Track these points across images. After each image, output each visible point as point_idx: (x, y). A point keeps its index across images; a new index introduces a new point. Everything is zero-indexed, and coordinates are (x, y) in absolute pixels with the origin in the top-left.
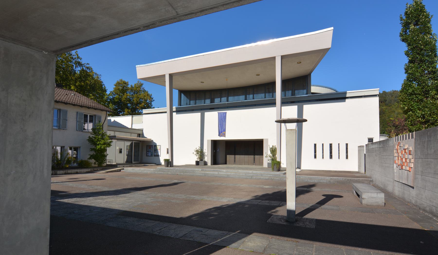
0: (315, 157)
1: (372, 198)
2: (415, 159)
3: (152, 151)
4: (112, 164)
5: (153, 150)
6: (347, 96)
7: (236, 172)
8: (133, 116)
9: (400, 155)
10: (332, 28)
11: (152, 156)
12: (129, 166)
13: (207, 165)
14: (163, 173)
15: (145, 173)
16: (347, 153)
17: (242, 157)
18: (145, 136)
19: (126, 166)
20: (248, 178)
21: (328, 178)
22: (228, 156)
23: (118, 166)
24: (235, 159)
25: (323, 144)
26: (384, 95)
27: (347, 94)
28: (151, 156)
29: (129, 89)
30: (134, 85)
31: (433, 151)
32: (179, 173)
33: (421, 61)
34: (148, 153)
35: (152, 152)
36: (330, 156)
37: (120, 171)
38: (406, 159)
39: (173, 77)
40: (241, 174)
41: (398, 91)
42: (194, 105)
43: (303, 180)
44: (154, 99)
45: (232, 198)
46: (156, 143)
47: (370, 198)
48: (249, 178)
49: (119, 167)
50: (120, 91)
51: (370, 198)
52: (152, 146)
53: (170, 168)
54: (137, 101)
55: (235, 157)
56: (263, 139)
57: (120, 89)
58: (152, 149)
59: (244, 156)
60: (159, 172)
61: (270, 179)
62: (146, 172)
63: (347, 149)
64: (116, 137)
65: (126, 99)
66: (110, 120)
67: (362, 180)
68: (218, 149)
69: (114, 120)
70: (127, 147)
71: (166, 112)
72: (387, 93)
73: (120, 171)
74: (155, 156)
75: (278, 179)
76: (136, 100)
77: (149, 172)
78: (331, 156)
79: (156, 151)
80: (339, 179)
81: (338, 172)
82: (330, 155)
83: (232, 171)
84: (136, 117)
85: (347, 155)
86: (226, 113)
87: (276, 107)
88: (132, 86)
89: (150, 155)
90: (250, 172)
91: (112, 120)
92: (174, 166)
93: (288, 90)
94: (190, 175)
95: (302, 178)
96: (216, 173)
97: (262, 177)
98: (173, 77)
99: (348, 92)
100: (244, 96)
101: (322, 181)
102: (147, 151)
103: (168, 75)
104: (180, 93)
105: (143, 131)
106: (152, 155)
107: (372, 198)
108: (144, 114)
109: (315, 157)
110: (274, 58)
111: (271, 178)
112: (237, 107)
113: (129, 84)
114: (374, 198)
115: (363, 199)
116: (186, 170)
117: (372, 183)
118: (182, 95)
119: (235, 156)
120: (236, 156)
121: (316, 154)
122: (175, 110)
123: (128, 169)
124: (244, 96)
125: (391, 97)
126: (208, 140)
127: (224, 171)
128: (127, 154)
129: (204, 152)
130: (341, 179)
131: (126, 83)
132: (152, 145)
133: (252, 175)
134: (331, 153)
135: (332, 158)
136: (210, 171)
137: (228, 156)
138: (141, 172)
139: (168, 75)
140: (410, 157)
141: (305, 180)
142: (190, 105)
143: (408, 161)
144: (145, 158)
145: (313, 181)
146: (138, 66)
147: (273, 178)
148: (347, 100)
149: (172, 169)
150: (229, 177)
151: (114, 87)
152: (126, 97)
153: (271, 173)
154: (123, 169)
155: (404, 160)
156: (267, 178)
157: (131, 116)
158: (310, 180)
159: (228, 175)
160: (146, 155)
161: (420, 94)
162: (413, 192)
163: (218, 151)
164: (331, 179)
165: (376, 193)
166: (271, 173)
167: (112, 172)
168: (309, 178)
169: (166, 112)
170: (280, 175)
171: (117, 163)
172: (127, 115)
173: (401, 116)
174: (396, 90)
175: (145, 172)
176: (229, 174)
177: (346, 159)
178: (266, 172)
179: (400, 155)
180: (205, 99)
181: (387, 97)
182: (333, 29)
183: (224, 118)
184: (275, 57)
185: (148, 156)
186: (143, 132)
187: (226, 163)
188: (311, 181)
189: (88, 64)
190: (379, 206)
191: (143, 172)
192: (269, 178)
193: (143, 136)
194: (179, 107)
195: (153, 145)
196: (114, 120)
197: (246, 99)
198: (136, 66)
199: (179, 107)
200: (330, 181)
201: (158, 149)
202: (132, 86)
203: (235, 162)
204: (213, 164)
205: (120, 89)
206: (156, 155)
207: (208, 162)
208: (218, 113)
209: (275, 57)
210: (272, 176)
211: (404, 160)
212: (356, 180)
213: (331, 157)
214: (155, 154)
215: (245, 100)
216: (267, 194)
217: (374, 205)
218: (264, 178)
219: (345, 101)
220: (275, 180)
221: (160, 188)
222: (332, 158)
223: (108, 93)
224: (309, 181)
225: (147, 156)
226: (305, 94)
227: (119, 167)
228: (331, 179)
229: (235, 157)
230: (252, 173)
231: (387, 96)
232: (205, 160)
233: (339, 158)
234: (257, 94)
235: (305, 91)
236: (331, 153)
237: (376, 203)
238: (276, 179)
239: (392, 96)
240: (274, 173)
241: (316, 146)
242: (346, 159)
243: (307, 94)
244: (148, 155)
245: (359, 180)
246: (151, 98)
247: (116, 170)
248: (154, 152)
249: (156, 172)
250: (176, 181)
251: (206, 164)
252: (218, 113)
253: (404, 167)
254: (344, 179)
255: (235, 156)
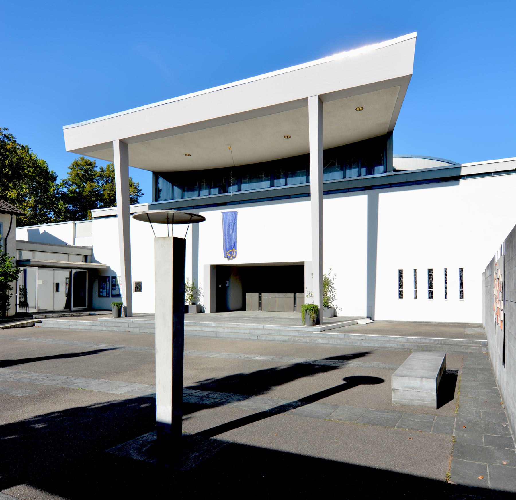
0: (401, 296)
1: (411, 388)
3: (108, 288)
4: (27, 312)
5: (109, 285)
6: (462, 174)
7: (235, 326)
8: (76, 222)
10: (414, 34)
11: (109, 297)
12: (57, 316)
13: (204, 312)
14: (104, 329)
15: (74, 329)
16: (462, 288)
17: (273, 296)
18: (97, 258)
19: (51, 316)
20: (252, 338)
21: (402, 339)
22: (248, 295)
23: (33, 315)
24: (260, 300)
25: (415, 271)
27: (463, 169)
28: (106, 297)
29: (95, 175)
30: (106, 167)
32: (131, 330)
34: (101, 290)
35: (109, 289)
36: (429, 293)
37: (34, 325)
39: (130, 146)
40: (242, 331)
42: (179, 200)
43: (352, 343)
44: (142, 192)
45: (147, 385)
46: (115, 272)
47: (406, 389)
48: (254, 338)
49: (36, 318)
50: (80, 178)
51: (406, 389)
52: (109, 277)
53: (127, 319)
54: (110, 195)
55: (260, 297)
56: (304, 262)
57: (81, 175)
58: (108, 283)
59: (276, 294)
60: (98, 328)
61: (292, 340)
62: (75, 328)
63: (461, 278)
64: (30, 261)
65: (90, 192)
66: (38, 230)
67: (468, 342)
68: (228, 282)
69: (45, 231)
70: (66, 280)
71: (115, 216)
73: (34, 325)
74: (113, 296)
75: (306, 340)
76: (109, 194)
77: (81, 327)
78: (430, 294)
79: (115, 287)
80: (423, 341)
81: (435, 325)
82: (429, 291)
83: (229, 326)
84: (81, 225)
85: (462, 291)
86: (236, 214)
87: (310, 200)
88: (102, 169)
89: (105, 294)
90: (260, 326)
91: (41, 231)
92: (133, 315)
93: (350, 168)
94: (150, 333)
95: (353, 338)
96: (198, 329)
97: (277, 338)
98: (129, 146)
99: (463, 165)
100: (269, 182)
101: (388, 345)
102: (99, 288)
103: (118, 141)
104: (155, 178)
105: (93, 250)
106: (109, 294)
107: (411, 388)
108: (95, 217)
109: (401, 296)
110: (305, 101)
111: (293, 338)
112: (240, 202)
113: (96, 165)
114: (415, 390)
115: (394, 390)
116: (146, 322)
117: (486, 349)
118: (161, 180)
119: (295, 294)
120: (263, 295)
121: (402, 291)
123: (48, 322)
124: (269, 182)
126: (205, 266)
127: (214, 324)
128: (67, 293)
129: (198, 288)
130: (428, 341)
131: (90, 164)
132: (109, 276)
133: (260, 332)
134: (431, 287)
135: (432, 298)
136: (189, 324)
137: (248, 295)
138: (68, 327)
139: (118, 142)
141: (356, 343)
142: (173, 199)
144: (97, 301)
145: (370, 345)
146: (67, 126)
147: (297, 339)
148: (462, 182)
149: (124, 321)
150: (217, 337)
151: (69, 171)
152: (90, 189)
153: (298, 328)
154: (41, 322)
156: (286, 338)
157: (72, 222)
158: (365, 343)
159: (217, 333)
160: (97, 294)
163: (227, 285)
164: (408, 340)
165: (420, 379)
166: (298, 328)
167: (16, 327)
168: (366, 339)
169: (115, 216)
170: (311, 332)
171: (39, 310)
172: (65, 220)
175: (75, 327)
176: (221, 330)
177: (460, 298)
178: (289, 327)
180: (200, 189)
182: (416, 36)
183: (232, 222)
184: (308, 98)
185: (102, 296)
186: (92, 253)
187: (243, 308)
188: (368, 345)
189: (5, 129)
190: (425, 407)
191: (71, 327)
192: (291, 339)
193: (93, 260)
194: (155, 203)
195: (111, 275)
196: (45, 231)
197: (272, 186)
198: (64, 127)
199: (155, 203)
200: (403, 345)
201: (119, 283)
202: (102, 169)
203: (260, 306)
204: (215, 311)
205: (81, 175)
206: (115, 294)
207: (205, 306)
208: (222, 213)
209: (308, 98)
210: (297, 334)
212: (455, 343)
213: (430, 295)
214: (114, 293)
215: (271, 187)
216: (241, 374)
217: (416, 404)
218: (282, 339)
219: (458, 184)
220: (300, 342)
221: (55, 360)
222: (432, 298)
223: (58, 182)
224: (364, 344)
225: (100, 296)
226: (382, 172)
227: (37, 317)
228: (408, 340)
229: (260, 297)
230: (264, 329)
232: (201, 303)
233: (446, 297)
234: (292, 177)
235: (381, 168)
236: (431, 287)
237: (419, 400)
238: (303, 340)
240: (302, 329)
241: (402, 273)
242: (460, 298)
243: (385, 172)
244: (101, 294)
245: (462, 342)
246: (137, 189)
247: (23, 324)
248: (112, 289)
249: (93, 328)
250: (103, 346)
251: (200, 310)
252: (222, 213)
254: (432, 341)
255: (295, 294)
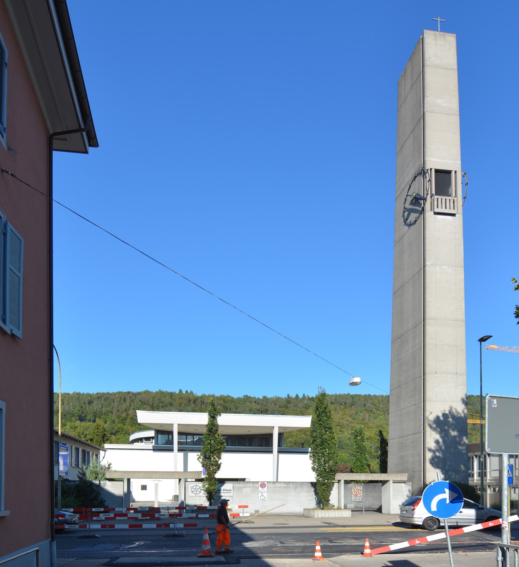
2: (363, 492)
9: (356, 491)
26: (265, 402)
31: (369, 490)
33: (361, 453)
38: (359, 493)
41: (282, 399)
72: (269, 400)
122: (152, 449)
125: (274, 406)
140: (361, 492)
143: (360, 493)
155: (358, 493)
161: (360, 467)
162: (361, 504)
173: (286, 434)
174: (281, 396)
179: (356, 491)
181: (269, 406)
194: (156, 445)
199: (156, 445)
211: (358, 493)
231: (269, 405)
239: (275, 405)
253: (357, 496)
